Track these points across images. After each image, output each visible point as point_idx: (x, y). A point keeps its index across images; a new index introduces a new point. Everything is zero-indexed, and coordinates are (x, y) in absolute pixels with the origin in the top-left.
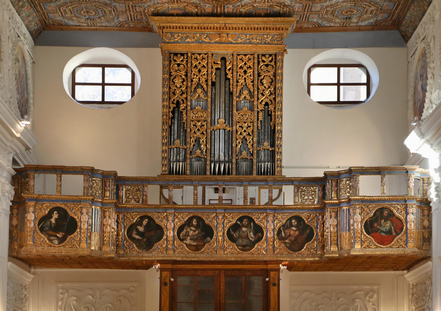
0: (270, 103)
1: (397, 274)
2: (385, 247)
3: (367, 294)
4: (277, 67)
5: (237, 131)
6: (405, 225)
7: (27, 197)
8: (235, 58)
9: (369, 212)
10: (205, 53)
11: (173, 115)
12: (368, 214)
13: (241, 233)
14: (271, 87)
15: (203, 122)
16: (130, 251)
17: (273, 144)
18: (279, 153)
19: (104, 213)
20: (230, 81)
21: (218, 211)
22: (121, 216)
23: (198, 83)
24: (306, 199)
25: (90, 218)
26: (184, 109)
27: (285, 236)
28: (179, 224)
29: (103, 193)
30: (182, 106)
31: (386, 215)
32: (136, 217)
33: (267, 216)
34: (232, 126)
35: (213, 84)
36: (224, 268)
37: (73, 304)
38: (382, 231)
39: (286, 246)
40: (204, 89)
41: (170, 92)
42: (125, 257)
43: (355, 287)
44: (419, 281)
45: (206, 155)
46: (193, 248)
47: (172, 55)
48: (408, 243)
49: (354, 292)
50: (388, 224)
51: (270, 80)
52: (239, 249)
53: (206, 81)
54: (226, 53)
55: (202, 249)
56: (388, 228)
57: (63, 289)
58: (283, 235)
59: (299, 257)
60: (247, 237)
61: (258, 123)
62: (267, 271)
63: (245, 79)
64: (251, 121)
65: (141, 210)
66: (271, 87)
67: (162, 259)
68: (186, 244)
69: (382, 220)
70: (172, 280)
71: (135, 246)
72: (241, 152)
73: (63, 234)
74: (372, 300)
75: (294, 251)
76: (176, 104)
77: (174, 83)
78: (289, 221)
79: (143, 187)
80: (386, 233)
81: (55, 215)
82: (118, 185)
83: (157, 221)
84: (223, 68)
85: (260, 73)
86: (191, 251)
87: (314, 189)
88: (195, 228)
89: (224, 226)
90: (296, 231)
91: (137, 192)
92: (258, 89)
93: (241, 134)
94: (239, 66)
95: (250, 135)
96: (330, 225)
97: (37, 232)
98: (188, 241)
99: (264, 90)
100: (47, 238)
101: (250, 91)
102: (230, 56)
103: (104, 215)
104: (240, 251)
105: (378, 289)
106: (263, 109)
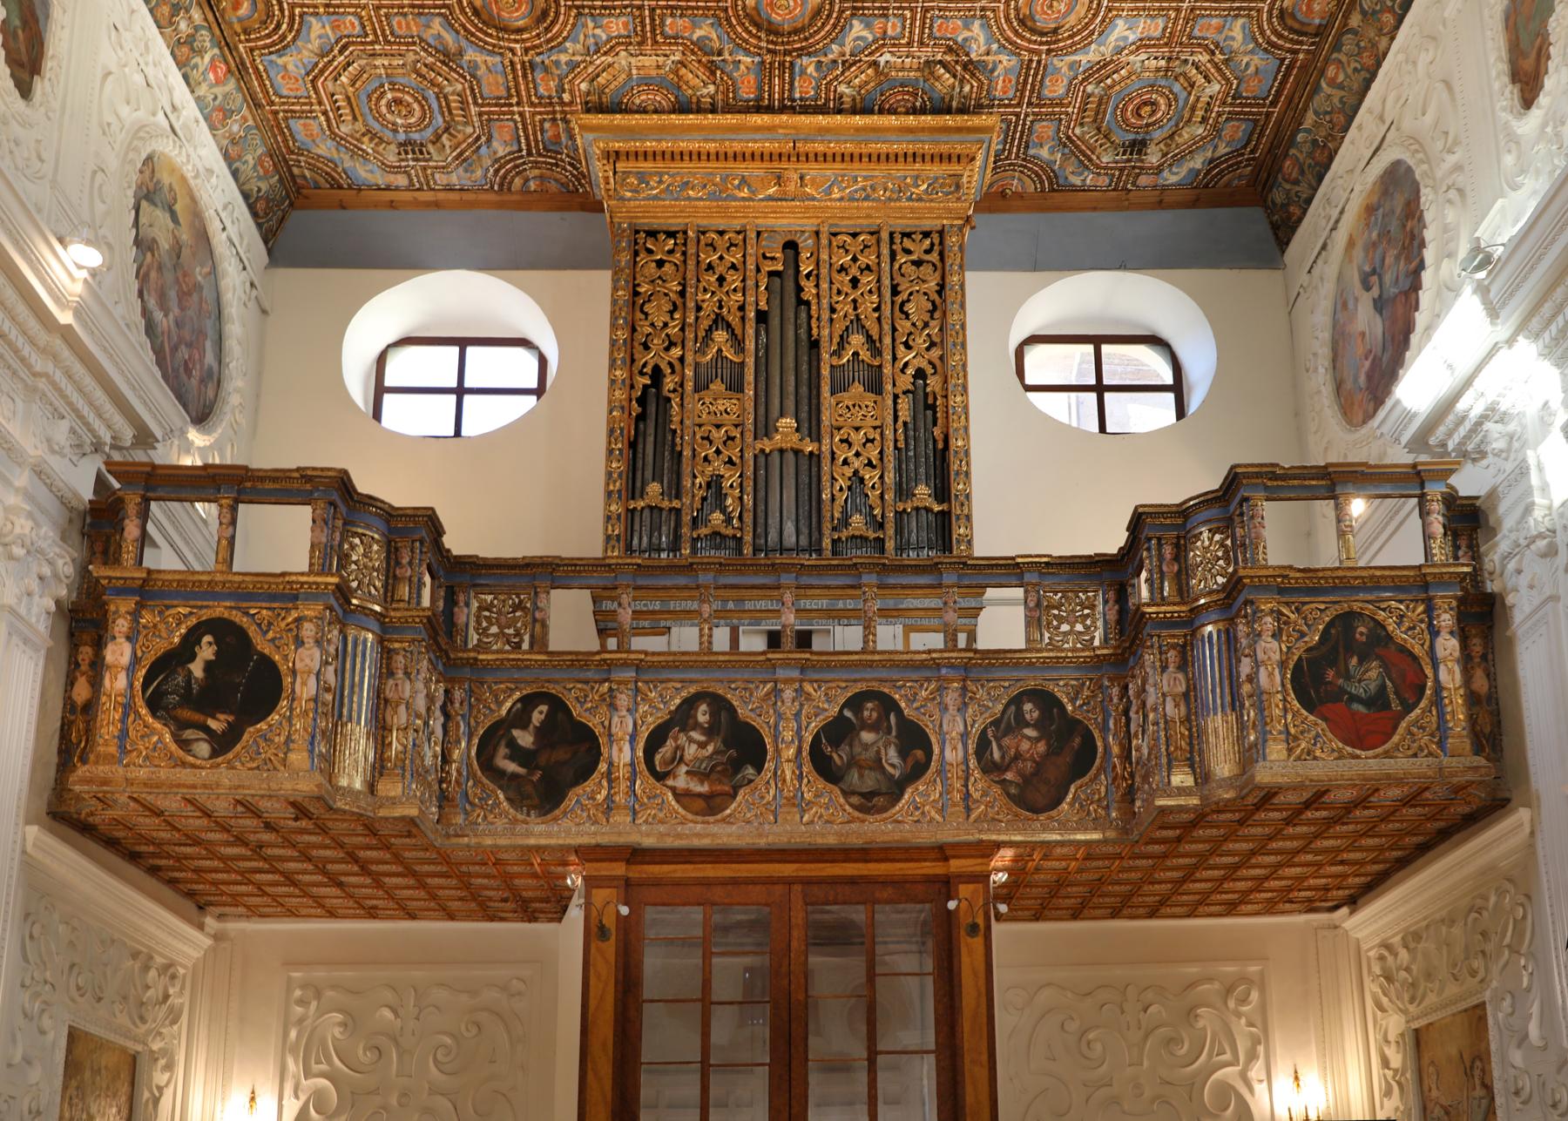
0: (930, 371)
1: (1315, 924)
2: (1370, 753)
3: (1229, 991)
4: (947, 268)
5: (833, 453)
6: (1429, 671)
7: (110, 578)
8: (824, 241)
9: (1305, 628)
10: (738, 228)
11: (640, 410)
12: (1303, 635)
13: (857, 749)
14: (932, 323)
15: (733, 428)
16: (485, 817)
17: (942, 493)
18: (963, 521)
19: (390, 658)
20: (809, 309)
21: (781, 674)
22: (458, 694)
23: (717, 315)
24: (1065, 634)
25: (327, 663)
26: (675, 391)
27: (1003, 757)
28: (650, 719)
29: (390, 588)
30: (669, 383)
31: (1364, 639)
32: (509, 696)
33: (939, 689)
34: (819, 441)
35: (762, 317)
36: (801, 874)
37: (334, 1038)
38: (1354, 698)
39: (1008, 794)
40: (733, 330)
41: (632, 340)
42: (467, 836)
43: (1193, 970)
44: (1425, 919)
45: (741, 529)
46: (700, 804)
47: (643, 235)
48: (1447, 738)
49: (1192, 985)
50: (1374, 672)
51: (930, 306)
52: (851, 805)
53: (742, 308)
54: (798, 228)
55: (727, 808)
56: (1373, 687)
57: (303, 987)
58: (997, 755)
59: (1053, 830)
60: (878, 764)
61: (895, 430)
62: (948, 882)
63: (855, 301)
64: (878, 423)
65: (525, 675)
66: (932, 323)
67: (593, 841)
68: (673, 790)
69: (1352, 657)
70: (624, 910)
71: (501, 796)
72: (845, 522)
73: (231, 718)
74: (1244, 1009)
75: (1036, 810)
76: (651, 377)
77: (646, 314)
78: (1013, 708)
79: (536, 593)
80: (1369, 702)
81: (204, 648)
82: (452, 587)
83: (577, 711)
84: (791, 272)
85: (898, 285)
86: (690, 816)
87: (1088, 598)
88: (703, 734)
89: (800, 728)
90: (1038, 740)
91: (513, 612)
92: (894, 329)
93: (845, 462)
94: (836, 267)
95: (874, 467)
96: (1164, 695)
97: (137, 713)
98: (681, 781)
99: (910, 334)
100: (173, 735)
101: (869, 338)
102: (809, 237)
103: (388, 668)
104: (856, 814)
105: (1262, 973)
106: (911, 387)
